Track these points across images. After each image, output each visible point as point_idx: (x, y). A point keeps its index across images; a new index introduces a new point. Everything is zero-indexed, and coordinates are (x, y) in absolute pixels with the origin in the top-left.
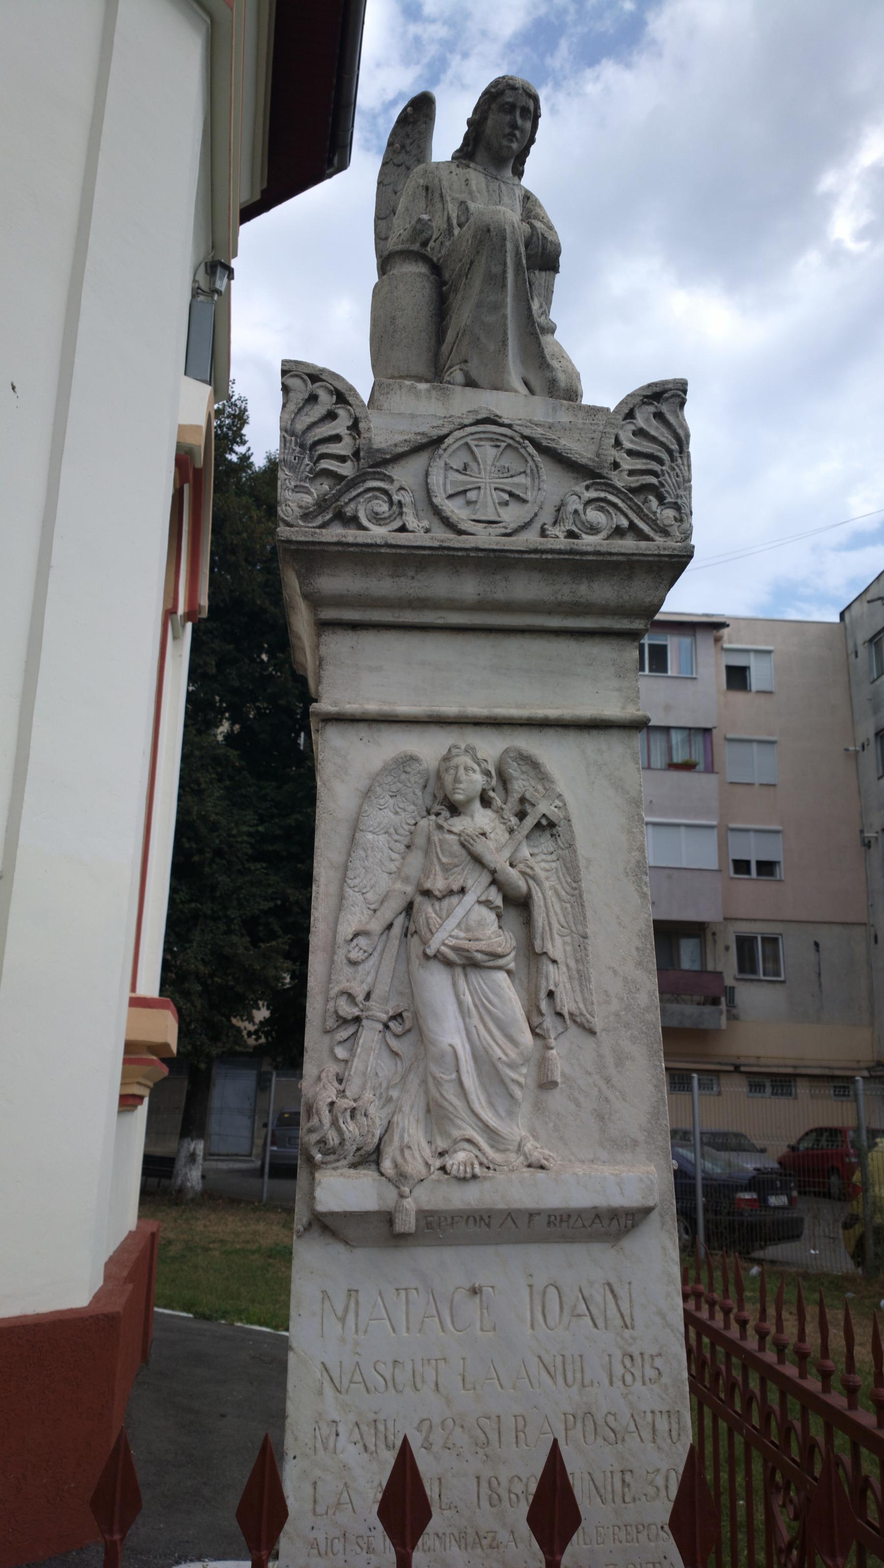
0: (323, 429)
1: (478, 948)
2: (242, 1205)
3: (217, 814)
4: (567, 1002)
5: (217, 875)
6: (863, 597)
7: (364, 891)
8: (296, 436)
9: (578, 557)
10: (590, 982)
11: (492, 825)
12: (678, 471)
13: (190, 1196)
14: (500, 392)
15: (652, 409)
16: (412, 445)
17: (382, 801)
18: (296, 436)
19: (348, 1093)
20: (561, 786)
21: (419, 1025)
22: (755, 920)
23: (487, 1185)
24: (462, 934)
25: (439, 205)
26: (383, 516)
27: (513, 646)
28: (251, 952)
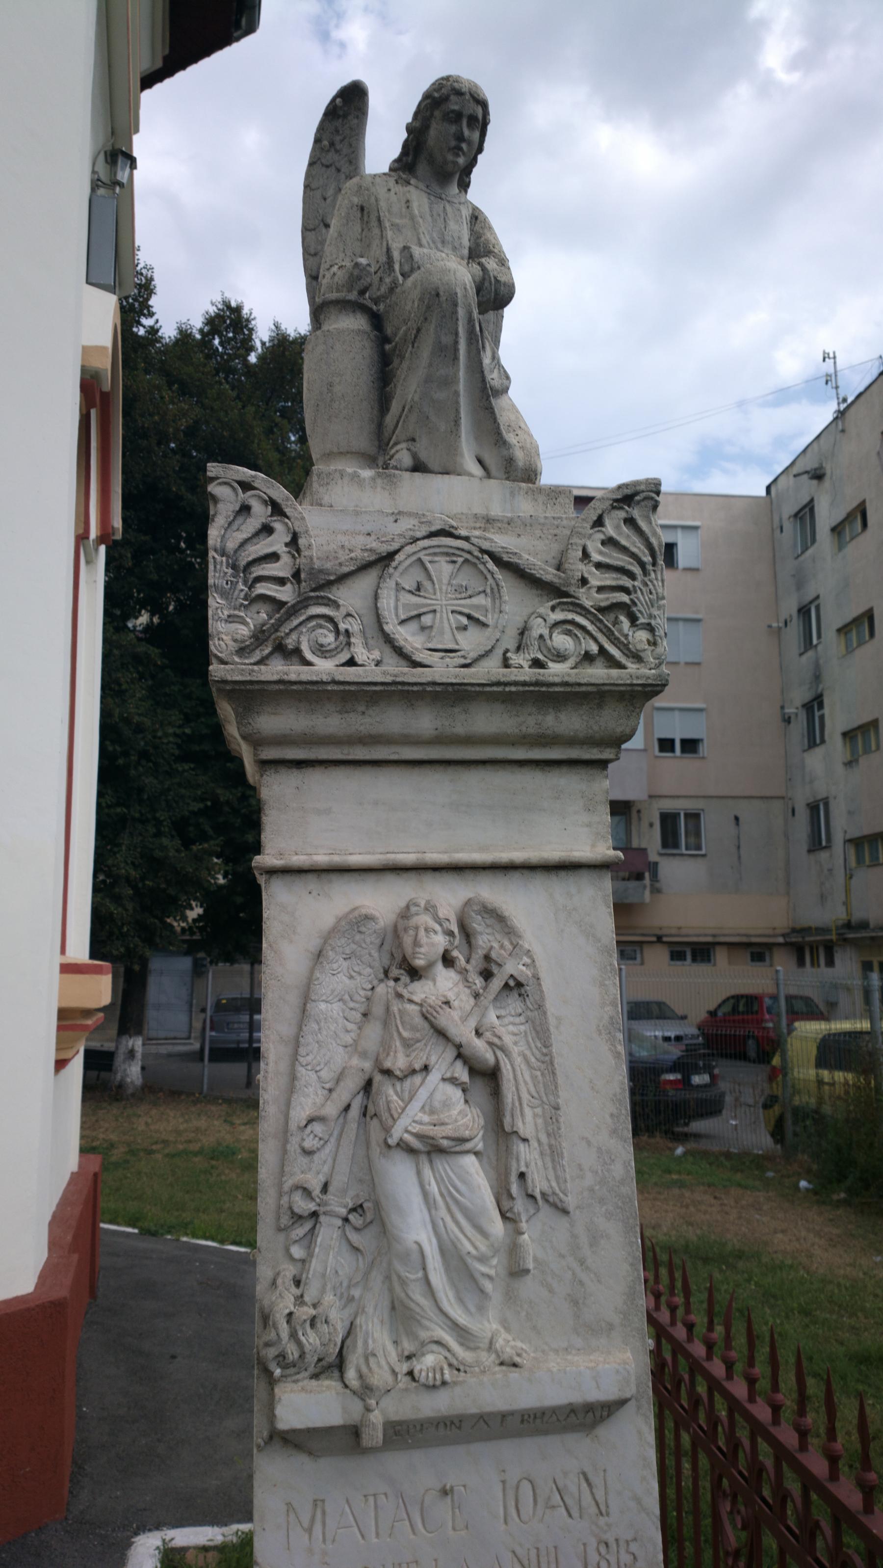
0: (258, 546)
1: (444, 1135)
2: (183, 1097)
3: (139, 715)
4: (538, 1182)
5: (143, 778)
6: (790, 470)
7: (318, 1068)
8: (228, 557)
9: (544, 689)
10: (563, 1158)
11: (456, 990)
12: (651, 587)
13: (130, 1091)
14: (452, 477)
15: (622, 514)
16: (358, 563)
17: (335, 966)
18: (228, 557)
19: (307, 1298)
20: (530, 940)
21: (380, 1215)
22: (678, 797)
23: (458, 1390)
24: (426, 1118)
25: (376, 231)
26: (328, 648)
27: (474, 778)
28: (183, 855)
